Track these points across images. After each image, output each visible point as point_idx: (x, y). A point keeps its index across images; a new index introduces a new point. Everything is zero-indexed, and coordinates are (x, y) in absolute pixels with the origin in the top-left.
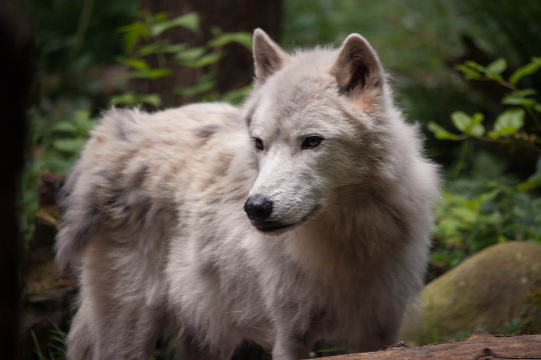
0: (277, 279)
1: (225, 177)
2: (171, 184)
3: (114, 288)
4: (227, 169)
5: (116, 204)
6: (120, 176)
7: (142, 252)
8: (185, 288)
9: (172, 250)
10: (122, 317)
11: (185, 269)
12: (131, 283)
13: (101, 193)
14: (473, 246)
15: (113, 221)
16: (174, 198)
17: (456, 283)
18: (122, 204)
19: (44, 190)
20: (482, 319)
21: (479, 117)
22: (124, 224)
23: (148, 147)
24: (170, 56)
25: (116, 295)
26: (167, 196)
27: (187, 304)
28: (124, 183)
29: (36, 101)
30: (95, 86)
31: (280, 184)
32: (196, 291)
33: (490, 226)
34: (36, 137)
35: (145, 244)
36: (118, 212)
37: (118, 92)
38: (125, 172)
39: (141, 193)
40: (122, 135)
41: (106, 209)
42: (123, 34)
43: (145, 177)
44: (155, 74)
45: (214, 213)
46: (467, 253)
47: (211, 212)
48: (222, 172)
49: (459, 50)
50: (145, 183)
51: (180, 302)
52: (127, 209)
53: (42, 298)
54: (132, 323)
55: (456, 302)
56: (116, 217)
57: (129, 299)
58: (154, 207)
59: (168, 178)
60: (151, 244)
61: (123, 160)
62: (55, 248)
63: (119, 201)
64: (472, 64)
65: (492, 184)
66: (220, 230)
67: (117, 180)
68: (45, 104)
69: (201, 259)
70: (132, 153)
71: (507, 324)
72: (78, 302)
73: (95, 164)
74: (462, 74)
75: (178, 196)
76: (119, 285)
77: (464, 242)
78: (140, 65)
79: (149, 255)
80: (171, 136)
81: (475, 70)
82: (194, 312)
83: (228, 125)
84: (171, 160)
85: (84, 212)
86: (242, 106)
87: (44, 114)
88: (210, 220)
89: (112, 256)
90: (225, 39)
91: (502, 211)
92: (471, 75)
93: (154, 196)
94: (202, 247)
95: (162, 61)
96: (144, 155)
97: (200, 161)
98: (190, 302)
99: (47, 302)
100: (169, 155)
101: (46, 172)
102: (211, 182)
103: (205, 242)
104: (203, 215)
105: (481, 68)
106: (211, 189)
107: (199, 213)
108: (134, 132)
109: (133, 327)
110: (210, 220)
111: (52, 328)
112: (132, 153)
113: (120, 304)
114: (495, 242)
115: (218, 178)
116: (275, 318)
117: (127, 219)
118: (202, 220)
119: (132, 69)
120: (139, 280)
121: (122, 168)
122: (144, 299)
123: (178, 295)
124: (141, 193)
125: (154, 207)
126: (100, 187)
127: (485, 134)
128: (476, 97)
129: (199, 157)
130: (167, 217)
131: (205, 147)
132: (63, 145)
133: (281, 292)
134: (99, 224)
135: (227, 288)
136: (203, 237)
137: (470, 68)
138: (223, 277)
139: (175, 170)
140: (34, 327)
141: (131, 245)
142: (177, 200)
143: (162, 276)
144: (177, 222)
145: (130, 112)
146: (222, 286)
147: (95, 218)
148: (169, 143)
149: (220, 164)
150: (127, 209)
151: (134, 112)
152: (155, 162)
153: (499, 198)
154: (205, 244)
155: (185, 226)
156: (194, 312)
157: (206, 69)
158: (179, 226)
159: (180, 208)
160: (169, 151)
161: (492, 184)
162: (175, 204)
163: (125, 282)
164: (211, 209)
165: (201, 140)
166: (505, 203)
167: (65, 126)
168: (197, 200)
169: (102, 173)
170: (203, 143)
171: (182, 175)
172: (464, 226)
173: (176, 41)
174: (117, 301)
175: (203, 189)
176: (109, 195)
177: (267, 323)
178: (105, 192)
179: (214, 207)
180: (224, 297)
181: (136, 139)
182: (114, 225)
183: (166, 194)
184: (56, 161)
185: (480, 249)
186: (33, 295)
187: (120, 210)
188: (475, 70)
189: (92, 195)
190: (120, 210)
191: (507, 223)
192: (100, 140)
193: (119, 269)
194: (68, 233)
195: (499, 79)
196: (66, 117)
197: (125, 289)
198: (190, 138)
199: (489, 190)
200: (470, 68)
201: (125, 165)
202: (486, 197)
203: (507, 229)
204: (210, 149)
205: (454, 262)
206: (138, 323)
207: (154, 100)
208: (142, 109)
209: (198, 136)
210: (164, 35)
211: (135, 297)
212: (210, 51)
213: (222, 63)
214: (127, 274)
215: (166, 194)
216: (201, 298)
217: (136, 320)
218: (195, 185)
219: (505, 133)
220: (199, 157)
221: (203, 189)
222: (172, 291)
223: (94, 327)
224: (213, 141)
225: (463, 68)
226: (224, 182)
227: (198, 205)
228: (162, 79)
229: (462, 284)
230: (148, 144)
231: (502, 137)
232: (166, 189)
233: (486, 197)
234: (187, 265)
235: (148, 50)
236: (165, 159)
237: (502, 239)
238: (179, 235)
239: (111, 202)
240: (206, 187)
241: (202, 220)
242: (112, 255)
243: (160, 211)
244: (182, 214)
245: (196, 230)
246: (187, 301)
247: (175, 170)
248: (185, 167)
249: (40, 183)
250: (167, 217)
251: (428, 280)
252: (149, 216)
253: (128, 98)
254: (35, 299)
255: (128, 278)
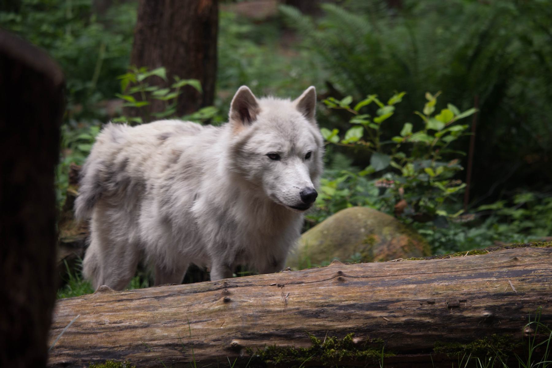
0: (216, 231)
1: (177, 164)
2: (142, 168)
3: (111, 233)
4: (178, 159)
5: (110, 181)
6: (112, 164)
7: (126, 211)
8: (150, 231)
9: (143, 208)
10: (116, 250)
11: (150, 219)
12: (121, 229)
13: (102, 175)
14: (332, 209)
15: (109, 191)
16: (144, 176)
17: (322, 232)
18: (114, 182)
19: (72, 175)
20: (337, 254)
21: (336, 131)
22: (115, 194)
23: (129, 146)
24: (148, 93)
25: (112, 237)
26: (140, 176)
27: (152, 241)
28: (115, 169)
29: (67, 121)
30: (103, 112)
31: (379, 267)
32: (156, 234)
33: (342, 197)
34: (67, 142)
35: (128, 206)
36: (111, 186)
37: (117, 116)
38: (115, 161)
39: (124, 174)
40: (114, 139)
41: (105, 184)
42: (121, 80)
43: (127, 164)
44: (139, 104)
45: (170, 186)
46: (329, 213)
47: (168, 185)
48: (175, 161)
49: (324, 91)
50: (127, 168)
51: (147, 240)
52: (117, 184)
53: (71, 241)
54: (122, 254)
55: (322, 243)
56: (110, 189)
57: (119, 239)
58: (133, 183)
59: (140, 164)
60: (131, 206)
61: (114, 154)
62: (74, 208)
63: (112, 179)
64: (332, 99)
65: (344, 172)
66: (173, 197)
67: (111, 167)
68: (73, 123)
69: (161, 214)
70: (120, 150)
71: (352, 257)
72: (89, 241)
73: (99, 157)
74: (325, 105)
75: (146, 176)
76: (113, 231)
77: (327, 207)
78: (130, 99)
79: (131, 212)
80: (143, 140)
81: (333, 102)
82: (156, 246)
83: (177, 132)
84: (143, 154)
85: (91, 186)
86: (232, 149)
87: (72, 129)
88: (167, 190)
89: (108, 214)
90: (182, 83)
91: (350, 188)
92: (332, 105)
93: (132, 176)
94: (162, 207)
95: (144, 97)
96: (126, 151)
97: (160, 154)
98: (153, 240)
99: (73, 243)
100: (141, 151)
101: (73, 164)
102: (168, 167)
103: (163, 203)
104: (162, 187)
105: (337, 102)
106: (168, 171)
107: (160, 186)
108: (121, 137)
109: (123, 257)
110: (167, 190)
111: (77, 258)
112: (120, 150)
113: (115, 243)
114: (345, 207)
115: (172, 165)
116: (211, 253)
117: (117, 191)
118: (162, 190)
119: (126, 101)
120: (125, 228)
121: (113, 159)
122: (127, 239)
123: (145, 236)
124: (124, 174)
125: (133, 183)
126: (101, 171)
127: (339, 142)
128: (334, 119)
129: (159, 151)
130: (140, 188)
131: (163, 145)
132: (83, 147)
133: (218, 238)
134: (101, 194)
135: (176, 232)
136: (162, 200)
137: (330, 101)
138: (174, 225)
139: (145, 159)
140: (66, 258)
141: (119, 207)
142: (145, 178)
143: (137, 224)
144: (146, 191)
145: (121, 126)
146: (173, 230)
147: (98, 190)
148: (141, 143)
149: (173, 157)
150: (117, 184)
151: (124, 126)
152: (133, 155)
153: (348, 180)
154: (164, 205)
155: (150, 193)
156: (156, 246)
157: (170, 101)
158: (146, 193)
159: (147, 182)
160: (142, 148)
161: (344, 172)
162: (144, 180)
163: (117, 229)
164: (167, 184)
165: (161, 141)
166: (351, 183)
167: (84, 136)
168: (159, 178)
169: (102, 163)
170: (162, 143)
171: (149, 163)
172: (327, 197)
173: (152, 85)
174: (112, 241)
175: (162, 171)
176: (106, 176)
177: (206, 256)
178: (104, 174)
179: (170, 182)
180: (174, 237)
181: (122, 142)
182: (109, 194)
183: (139, 175)
184: (79, 157)
185: (336, 211)
186: (65, 238)
187: (112, 185)
188: (333, 102)
189: (97, 176)
190: (112, 185)
191: (353, 195)
192: (102, 143)
193: (113, 222)
194: (82, 199)
195: (348, 108)
196: (86, 130)
197: (118, 233)
198: (154, 140)
199: (341, 175)
200: (330, 101)
201: (115, 157)
202: (340, 180)
203: (352, 200)
204: (166, 147)
205: (321, 219)
206: (126, 253)
207: (139, 120)
208: (128, 124)
209: (159, 139)
210: (145, 80)
211: (122, 238)
212: (172, 90)
213: (180, 98)
214: (118, 225)
215: (139, 174)
216: (160, 237)
217: (124, 252)
218: (157, 169)
219: (351, 141)
220: (159, 151)
221: (162, 171)
222: (143, 233)
223: (100, 257)
224: (168, 142)
225: (326, 101)
226: (176, 167)
227: (159, 181)
228: (143, 108)
229: (325, 232)
230: (129, 144)
231: (350, 143)
232: (140, 172)
233: (340, 180)
234: (152, 217)
235: (135, 90)
236: (138, 153)
237: (349, 205)
238: (147, 199)
239: (107, 180)
240: (164, 170)
241: (162, 190)
242: (109, 213)
243: (136, 185)
244: (148, 187)
245: (158, 196)
246: (151, 240)
247: (145, 159)
248: (150, 157)
249: (69, 170)
250: (140, 188)
251: (303, 231)
252: (130, 188)
253: (123, 119)
254: (67, 241)
255: (119, 227)
